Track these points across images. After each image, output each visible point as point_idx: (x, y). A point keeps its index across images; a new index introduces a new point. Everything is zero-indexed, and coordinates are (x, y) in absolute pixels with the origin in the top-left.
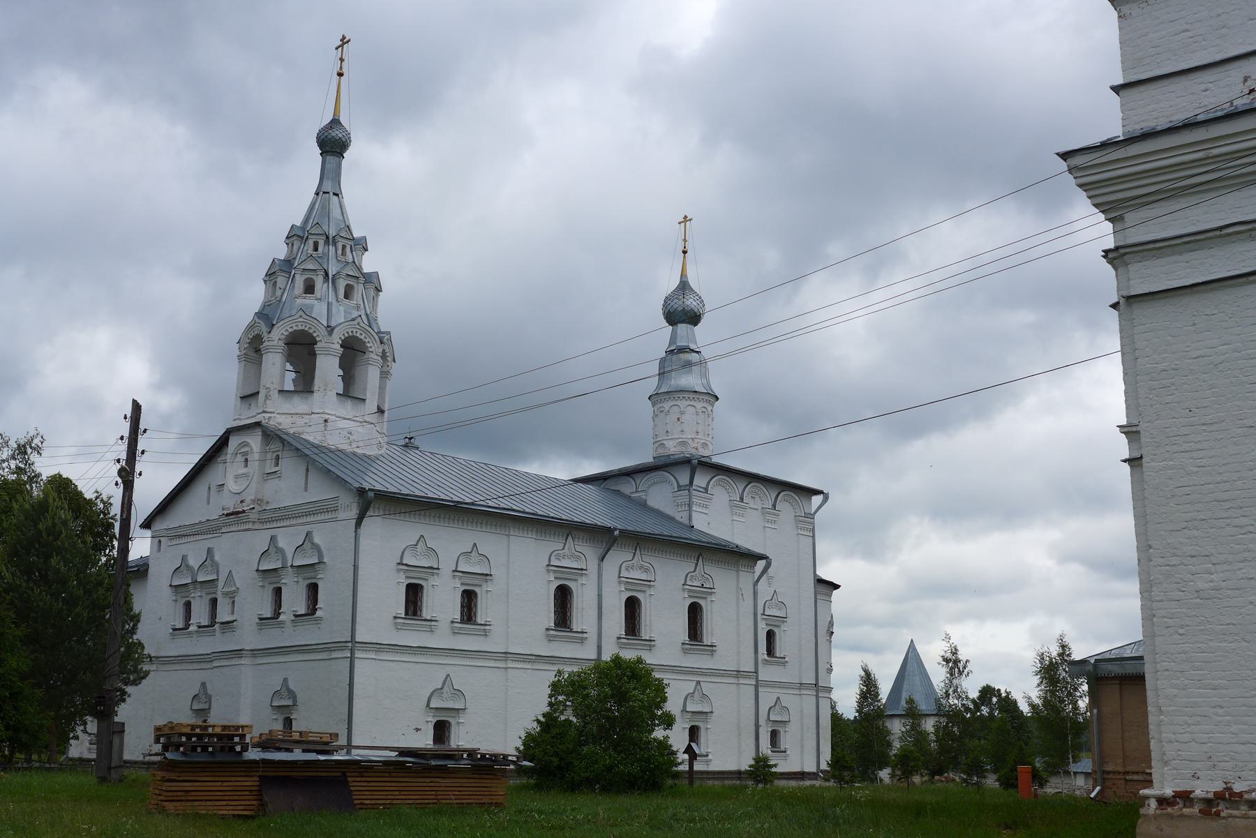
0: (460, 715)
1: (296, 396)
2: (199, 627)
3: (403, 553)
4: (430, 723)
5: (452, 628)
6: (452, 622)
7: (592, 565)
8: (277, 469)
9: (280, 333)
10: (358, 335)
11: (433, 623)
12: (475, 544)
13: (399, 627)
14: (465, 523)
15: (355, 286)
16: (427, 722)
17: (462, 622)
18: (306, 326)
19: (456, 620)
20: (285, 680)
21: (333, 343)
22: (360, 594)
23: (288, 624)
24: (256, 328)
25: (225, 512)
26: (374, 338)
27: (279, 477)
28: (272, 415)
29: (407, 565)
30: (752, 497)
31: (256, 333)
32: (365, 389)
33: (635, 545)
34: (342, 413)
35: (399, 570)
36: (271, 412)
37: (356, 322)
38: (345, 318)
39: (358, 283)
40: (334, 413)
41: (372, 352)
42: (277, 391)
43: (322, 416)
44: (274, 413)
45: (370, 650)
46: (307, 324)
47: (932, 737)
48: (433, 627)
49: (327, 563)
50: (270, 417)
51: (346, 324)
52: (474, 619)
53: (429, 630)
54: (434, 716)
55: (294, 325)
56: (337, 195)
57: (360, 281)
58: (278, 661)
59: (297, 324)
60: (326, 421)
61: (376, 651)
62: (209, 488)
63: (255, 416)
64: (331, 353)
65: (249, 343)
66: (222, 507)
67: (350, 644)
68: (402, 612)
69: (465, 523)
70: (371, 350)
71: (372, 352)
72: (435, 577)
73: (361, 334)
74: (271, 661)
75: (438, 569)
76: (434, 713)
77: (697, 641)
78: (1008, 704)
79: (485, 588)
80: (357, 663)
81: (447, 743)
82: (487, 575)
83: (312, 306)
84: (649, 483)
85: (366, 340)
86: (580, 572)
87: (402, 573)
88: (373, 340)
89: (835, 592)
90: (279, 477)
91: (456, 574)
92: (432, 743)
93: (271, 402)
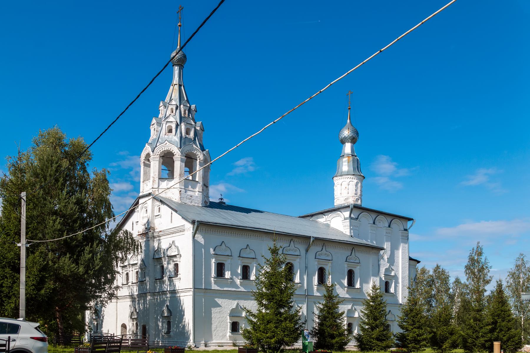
2: (132, 283)
7: (303, 252)
22: (203, 21)
24: (148, 150)
25: (139, 234)
30: (379, 222)
31: (147, 153)
33: (323, 244)
47: (345, 165)
50: (155, 191)
52: (248, 278)
62: (133, 223)
66: (138, 231)
77: (352, 286)
84: (332, 217)
86: (297, 256)
89: (418, 265)
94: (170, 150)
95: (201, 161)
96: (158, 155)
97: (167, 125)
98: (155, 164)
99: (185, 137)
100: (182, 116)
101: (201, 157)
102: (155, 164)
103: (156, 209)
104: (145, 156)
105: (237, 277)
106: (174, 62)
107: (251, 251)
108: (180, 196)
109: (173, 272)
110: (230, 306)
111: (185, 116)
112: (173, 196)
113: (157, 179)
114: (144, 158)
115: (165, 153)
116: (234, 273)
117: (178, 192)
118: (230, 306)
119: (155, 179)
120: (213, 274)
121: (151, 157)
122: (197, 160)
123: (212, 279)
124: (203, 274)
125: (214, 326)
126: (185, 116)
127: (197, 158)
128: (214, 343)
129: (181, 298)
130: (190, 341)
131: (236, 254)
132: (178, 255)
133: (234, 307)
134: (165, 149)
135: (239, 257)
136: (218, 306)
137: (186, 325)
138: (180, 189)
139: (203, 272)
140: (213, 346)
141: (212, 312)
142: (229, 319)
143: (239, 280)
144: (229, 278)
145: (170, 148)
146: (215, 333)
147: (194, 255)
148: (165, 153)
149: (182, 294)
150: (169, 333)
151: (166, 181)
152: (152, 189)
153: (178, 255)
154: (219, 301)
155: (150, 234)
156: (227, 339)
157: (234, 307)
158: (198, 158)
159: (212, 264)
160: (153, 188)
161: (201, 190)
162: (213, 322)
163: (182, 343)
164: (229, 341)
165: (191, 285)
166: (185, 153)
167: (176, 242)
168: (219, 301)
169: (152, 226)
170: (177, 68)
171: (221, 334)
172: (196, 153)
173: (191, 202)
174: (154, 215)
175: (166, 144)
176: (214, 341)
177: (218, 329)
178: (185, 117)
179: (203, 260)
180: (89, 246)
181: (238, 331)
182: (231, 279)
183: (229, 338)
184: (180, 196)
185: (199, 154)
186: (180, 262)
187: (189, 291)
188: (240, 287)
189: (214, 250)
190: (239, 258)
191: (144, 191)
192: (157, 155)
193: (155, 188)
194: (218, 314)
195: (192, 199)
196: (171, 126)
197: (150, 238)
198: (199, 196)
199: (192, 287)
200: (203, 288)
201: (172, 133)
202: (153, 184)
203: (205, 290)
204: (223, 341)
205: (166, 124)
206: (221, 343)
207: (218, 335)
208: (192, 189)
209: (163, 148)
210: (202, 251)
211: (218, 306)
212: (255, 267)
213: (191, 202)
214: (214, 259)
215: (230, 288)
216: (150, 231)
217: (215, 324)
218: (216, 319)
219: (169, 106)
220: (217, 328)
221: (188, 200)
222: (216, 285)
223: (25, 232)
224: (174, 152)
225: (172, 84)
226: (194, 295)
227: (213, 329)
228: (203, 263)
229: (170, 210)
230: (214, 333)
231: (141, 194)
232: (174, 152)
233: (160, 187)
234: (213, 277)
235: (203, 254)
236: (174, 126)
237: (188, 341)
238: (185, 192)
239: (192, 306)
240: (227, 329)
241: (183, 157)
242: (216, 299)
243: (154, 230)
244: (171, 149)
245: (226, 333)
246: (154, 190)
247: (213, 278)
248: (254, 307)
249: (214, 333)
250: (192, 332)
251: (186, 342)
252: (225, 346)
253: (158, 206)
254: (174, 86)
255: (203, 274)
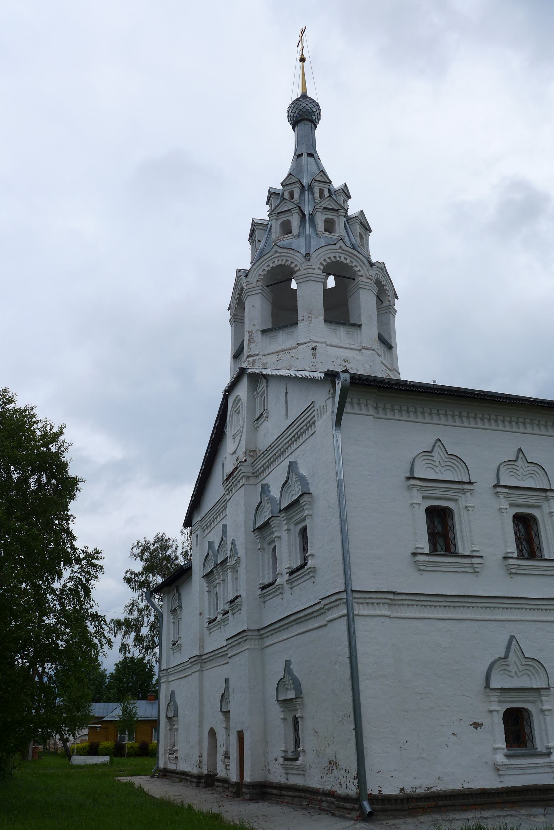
0: (544, 698)
1: (281, 332)
3: (413, 464)
4: (495, 714)
5: (508, 568)
6: (505, 558)
9: (258, 274)
10: (342, 259)
11: (475, 560)
12: (520, 450)
13: (422, 568)
14: (500, 423)
15: (336, 219)
16: (491, 712)
17: (521, 557)
18: (282, 260)
19: (510, 555)
20: (288, 664)
21: (314, 269)
23: (286, 586)
26: (362, 261)
28: (256, 357)
32: (360, 316)
34: (334, 341)
35: (410, 488)
36: (255, 355)
37: (337, 246)
38: (325, 243)
39: (338, 216)
40: (324, 341)
41: (362, 276)
42: (259, 332)
43: (309, 344)
44: (258, 355)
45: (378, 604)
48: (475, 566)
49: (313, 493)
51: (329, 247)
52: (538, 553)
53: (471, 570)
54: (500, 702)
55: (270, 263)
56: (311, 155)
57: (340, 213)
58: (281, 639)
59: (273, 260)
60: (314, 349)
64: (311, 278)
67: (344, 595)
68: (424, 545)
69: (500, 423)
70: (359, 273)
71: (362, 276)
72: (468, 494)
73: (346, 259)
74: (275, 641)
75: (471, 483)
76: (499, 696)
79: (546, 509)
80: (359, 623)
81: (529, 744)
82: (546, 490)
83: (291, 243)
85: (353, 265)
87: (415, 490)
88: (361, 263)
91: (499, 490)
92: (504, 746)
93: (254, 344)
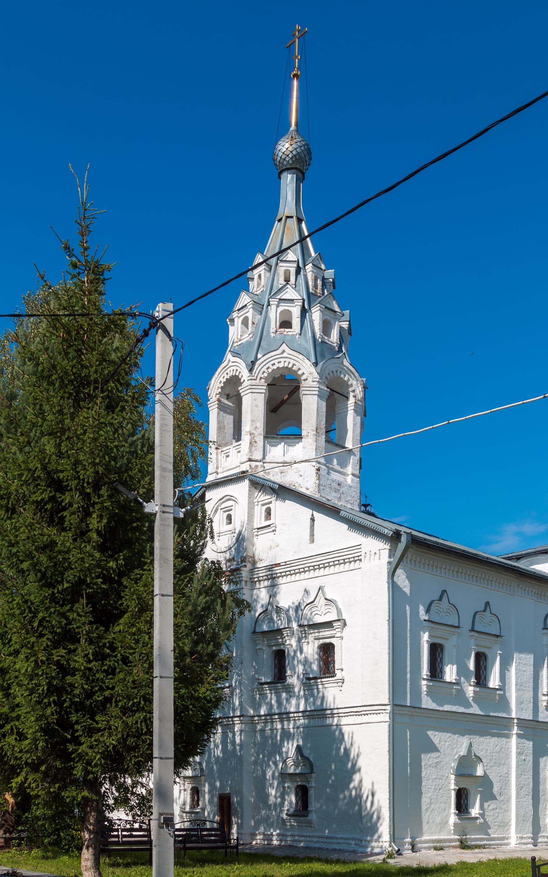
8: (268, 523)
24: (231, 369)
27: (273, 531)
29: (478, 632)
31: (230, 374)
45: (370, 714)
46: (291, 361)
50: (257, 466)
61: (410, 715)
63: (239, 466)
65: (222, 388)
78: (184, 768)
90: (273, 531)
94: (291, 369)
95: (358, 400)
96: (263, 380)
97: (280, 309)
98: (255, 400)
99: (322, 341)
100: (311, 291)
101: (357, 392)
102: (255, 400)
103: (259, 512)
104: (222, 385)
105: (468, 680)
106: (285, 163)
107: (494, 618)
108: (317, 482)
109: (316, 662)
110: (455, 751)
111: (315, 291)
112: (300, 480)
113: (260, 439)
114: (220, 390)
115: (274, 377)
116: (462, 671)
117: (314, 471)
118: (455, 751)
119: (257, 439)
120: (425, 671)
121: (244, 385)
122: (347, 398)
123: (424, 683)
124: (408, 670)
125: (425, 800)
126: (315, 291)
127: (348, 393)
128: (426, 842)
129: (345, 729)
130: (379, 837)
131: (466, 624)
132: (339, 620)
133: (462, 754)
134: (281, 365)
135: (473, 630)
136: (434, 749)
137: (364, 797)
138: (318, 465)
139: (408, 663)
140: (425, 848)
141: (423, 764)
142: (453, 782)
143: (471, 688)
144: (454, 681)
145: (292, 362)
146: (429, 817)
147: (393, 621)
148: (274, 377)
149: (344, 721)
150: (307, 816)
151: (283, 444)
152: (249, 463)
153: (339, 620)
154: (436, 737)
155: (245, 573)
156: (449, 833)
157: (463, 752)
158: (352, 394)
159: (423, 646)
160: (250, 460)
161: (357, 472)
162: (424, 790)
163: (349, 841)
164: (453, 837)
165: (384, 697)
166: (326, 377)
167: (326, 589)
168: (436, 737)
169: (250, 554)
170: (292, 178)
171: (438, 820)
172: (349, 380)
173: (340, 498)
174: (253, 526)
175: (284, 351)
176: (425, 838)
177: (433, 806)
178: (315, 295)
179: (408, 635)
180: (83, 598)
181: (465, 811)
182: (458, 683)
183: (452, 828)
184: (317, 482)
185: (354, 383)
186: (342, 638)
187: (377, 713)
188: (472, 703)
189: (428, 611)
190: (472, 633)
191: (219, 471)
192: (261, 378)
193: (256, 461)
194: (434, 769)
195: (341, 492)
196: (288, 310)
197: (243, 583)
198: (355, 485)
199: (387, 702)
200: (408, 705)
201: (291, 328)
202: (251, 451)
203: (412, 710)
204: (442, 837)
205: (277, 306)
206: (439, 841)
207: (433, 822)
208: (338, 468)
209: (276, 362)
210: (406, 611)
211: (434, 749)
212: (498, 658)
213: (340, 498)
214: (427, 634)
215: (455, 705)
216: (246, 566)
217: (428, 795)
218: (430, 782)
219: (281, 264)
220: (431, 804)
221: (333, 494)
222: (429, 699)
223: (172, 460)
224: (303, 374)
225: (278, 218)
226: (393, 721)
227: (424, 808)
228: (408, 642)
229: (306, 512)
230: (425, 817)
231: (210, 478)
232: (303, 374)
233: (267, 459)
234: (425, 677)
235: (408, 620)
236: (296, 311)
237: (372, 836)
238: (328, 473)
239: (387, 749)
240: (450, 808)
241: (322, 387)
242: (430, 733)
243: (254, 563)
244: (294, 365)
245: (448, 816)
246: (254, 464)
247: (424, 679)
248: (496, 752)
249: (427, 815)
250: (386, 813)
251: (365, 841)
252: (449, 847)
253: (263, 505)
254: (286, 220)
255: (408, 670)
